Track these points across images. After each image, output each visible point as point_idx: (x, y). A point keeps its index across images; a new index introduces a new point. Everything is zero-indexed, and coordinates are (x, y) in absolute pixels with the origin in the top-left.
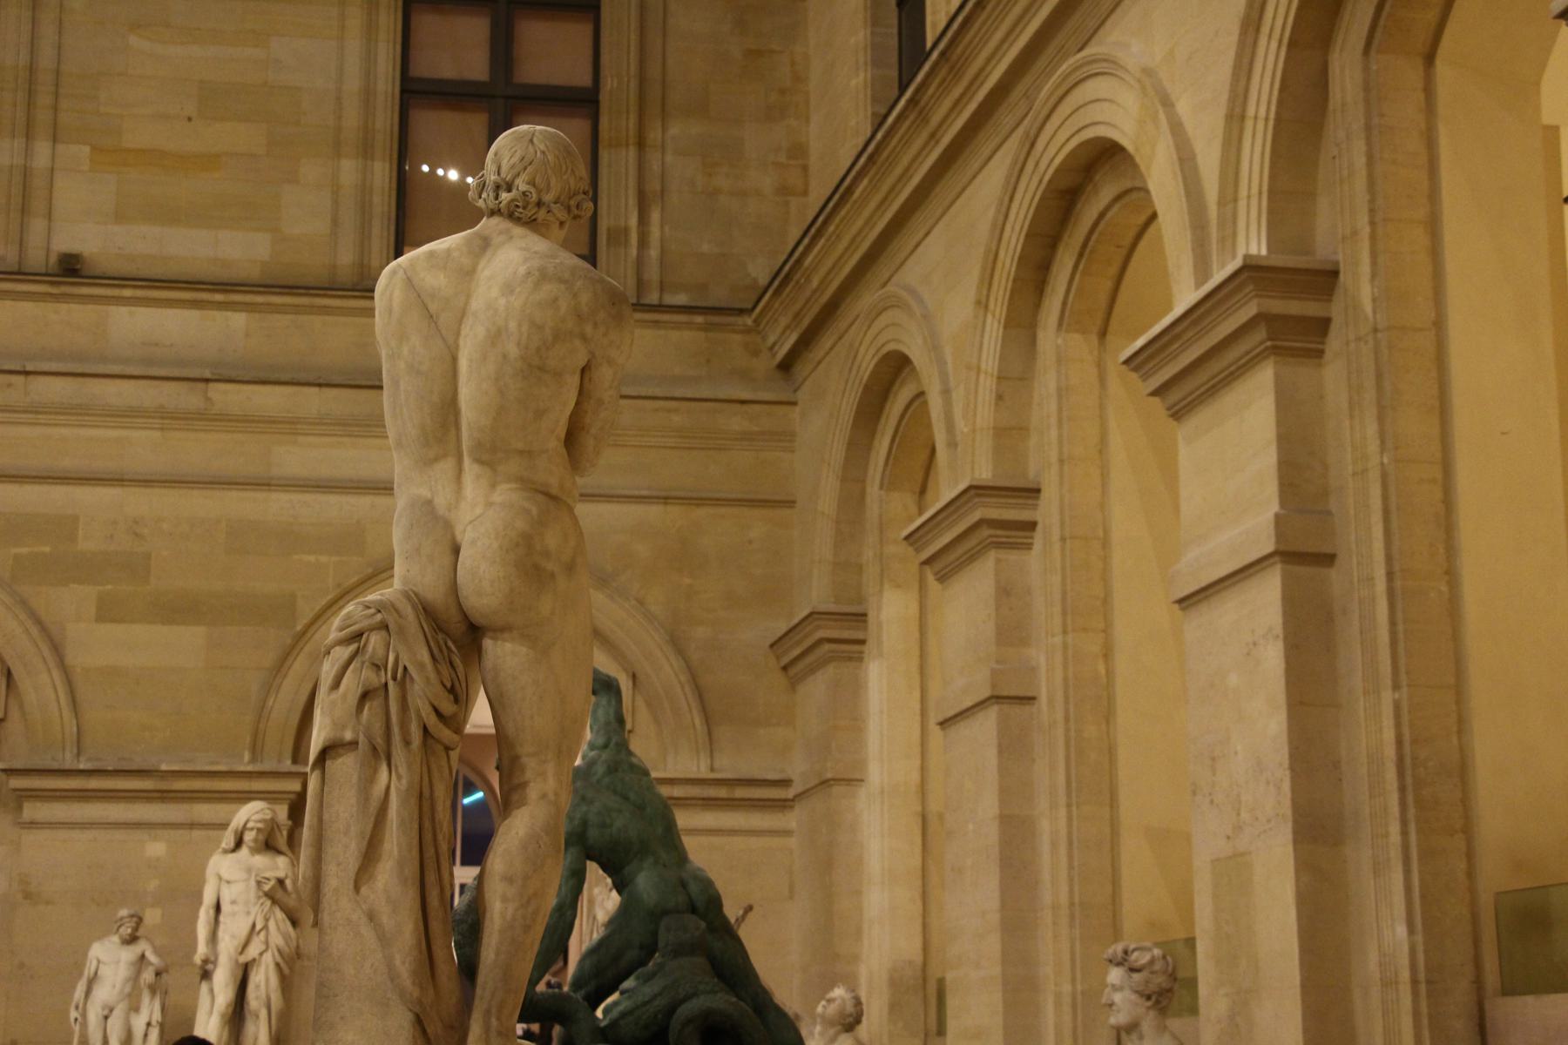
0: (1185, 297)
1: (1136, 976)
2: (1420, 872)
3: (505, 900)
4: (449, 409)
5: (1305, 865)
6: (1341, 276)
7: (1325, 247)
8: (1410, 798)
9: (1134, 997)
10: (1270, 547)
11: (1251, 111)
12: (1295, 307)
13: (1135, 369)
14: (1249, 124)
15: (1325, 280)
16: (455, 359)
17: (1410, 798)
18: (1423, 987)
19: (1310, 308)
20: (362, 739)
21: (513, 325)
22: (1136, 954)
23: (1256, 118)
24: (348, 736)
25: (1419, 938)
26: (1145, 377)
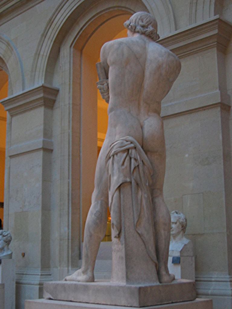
0: (17, 92)
1: (5, 238)
2: (72, 217)
3: (164, 230)
4: (140, 86)
5: (43, 214)
6: (60, 91)
7: (56, 84)
8: (70, 202)
9: (3, 242)
10: (41, 147)
11: (42, 53)
12: (50, 97)
13: (3, 104)
14: (40, 58)
15: (56, 92)
16: (144, 72)
17: (70, 202)
18: (70, 241)
19: (53, 98)
20: (133, 181)
21: (164, 66)
22: (4, 233)
23: (43, 55)
24: (128, 180)
25: (70, 230)
26: (5, 107)
